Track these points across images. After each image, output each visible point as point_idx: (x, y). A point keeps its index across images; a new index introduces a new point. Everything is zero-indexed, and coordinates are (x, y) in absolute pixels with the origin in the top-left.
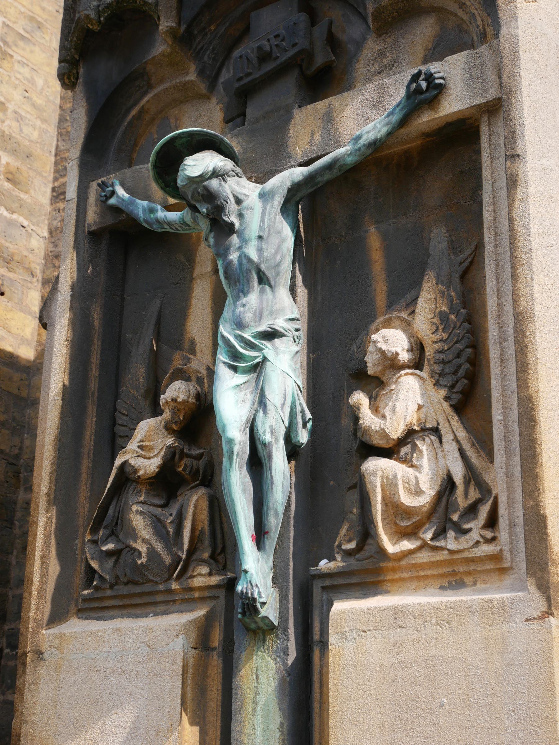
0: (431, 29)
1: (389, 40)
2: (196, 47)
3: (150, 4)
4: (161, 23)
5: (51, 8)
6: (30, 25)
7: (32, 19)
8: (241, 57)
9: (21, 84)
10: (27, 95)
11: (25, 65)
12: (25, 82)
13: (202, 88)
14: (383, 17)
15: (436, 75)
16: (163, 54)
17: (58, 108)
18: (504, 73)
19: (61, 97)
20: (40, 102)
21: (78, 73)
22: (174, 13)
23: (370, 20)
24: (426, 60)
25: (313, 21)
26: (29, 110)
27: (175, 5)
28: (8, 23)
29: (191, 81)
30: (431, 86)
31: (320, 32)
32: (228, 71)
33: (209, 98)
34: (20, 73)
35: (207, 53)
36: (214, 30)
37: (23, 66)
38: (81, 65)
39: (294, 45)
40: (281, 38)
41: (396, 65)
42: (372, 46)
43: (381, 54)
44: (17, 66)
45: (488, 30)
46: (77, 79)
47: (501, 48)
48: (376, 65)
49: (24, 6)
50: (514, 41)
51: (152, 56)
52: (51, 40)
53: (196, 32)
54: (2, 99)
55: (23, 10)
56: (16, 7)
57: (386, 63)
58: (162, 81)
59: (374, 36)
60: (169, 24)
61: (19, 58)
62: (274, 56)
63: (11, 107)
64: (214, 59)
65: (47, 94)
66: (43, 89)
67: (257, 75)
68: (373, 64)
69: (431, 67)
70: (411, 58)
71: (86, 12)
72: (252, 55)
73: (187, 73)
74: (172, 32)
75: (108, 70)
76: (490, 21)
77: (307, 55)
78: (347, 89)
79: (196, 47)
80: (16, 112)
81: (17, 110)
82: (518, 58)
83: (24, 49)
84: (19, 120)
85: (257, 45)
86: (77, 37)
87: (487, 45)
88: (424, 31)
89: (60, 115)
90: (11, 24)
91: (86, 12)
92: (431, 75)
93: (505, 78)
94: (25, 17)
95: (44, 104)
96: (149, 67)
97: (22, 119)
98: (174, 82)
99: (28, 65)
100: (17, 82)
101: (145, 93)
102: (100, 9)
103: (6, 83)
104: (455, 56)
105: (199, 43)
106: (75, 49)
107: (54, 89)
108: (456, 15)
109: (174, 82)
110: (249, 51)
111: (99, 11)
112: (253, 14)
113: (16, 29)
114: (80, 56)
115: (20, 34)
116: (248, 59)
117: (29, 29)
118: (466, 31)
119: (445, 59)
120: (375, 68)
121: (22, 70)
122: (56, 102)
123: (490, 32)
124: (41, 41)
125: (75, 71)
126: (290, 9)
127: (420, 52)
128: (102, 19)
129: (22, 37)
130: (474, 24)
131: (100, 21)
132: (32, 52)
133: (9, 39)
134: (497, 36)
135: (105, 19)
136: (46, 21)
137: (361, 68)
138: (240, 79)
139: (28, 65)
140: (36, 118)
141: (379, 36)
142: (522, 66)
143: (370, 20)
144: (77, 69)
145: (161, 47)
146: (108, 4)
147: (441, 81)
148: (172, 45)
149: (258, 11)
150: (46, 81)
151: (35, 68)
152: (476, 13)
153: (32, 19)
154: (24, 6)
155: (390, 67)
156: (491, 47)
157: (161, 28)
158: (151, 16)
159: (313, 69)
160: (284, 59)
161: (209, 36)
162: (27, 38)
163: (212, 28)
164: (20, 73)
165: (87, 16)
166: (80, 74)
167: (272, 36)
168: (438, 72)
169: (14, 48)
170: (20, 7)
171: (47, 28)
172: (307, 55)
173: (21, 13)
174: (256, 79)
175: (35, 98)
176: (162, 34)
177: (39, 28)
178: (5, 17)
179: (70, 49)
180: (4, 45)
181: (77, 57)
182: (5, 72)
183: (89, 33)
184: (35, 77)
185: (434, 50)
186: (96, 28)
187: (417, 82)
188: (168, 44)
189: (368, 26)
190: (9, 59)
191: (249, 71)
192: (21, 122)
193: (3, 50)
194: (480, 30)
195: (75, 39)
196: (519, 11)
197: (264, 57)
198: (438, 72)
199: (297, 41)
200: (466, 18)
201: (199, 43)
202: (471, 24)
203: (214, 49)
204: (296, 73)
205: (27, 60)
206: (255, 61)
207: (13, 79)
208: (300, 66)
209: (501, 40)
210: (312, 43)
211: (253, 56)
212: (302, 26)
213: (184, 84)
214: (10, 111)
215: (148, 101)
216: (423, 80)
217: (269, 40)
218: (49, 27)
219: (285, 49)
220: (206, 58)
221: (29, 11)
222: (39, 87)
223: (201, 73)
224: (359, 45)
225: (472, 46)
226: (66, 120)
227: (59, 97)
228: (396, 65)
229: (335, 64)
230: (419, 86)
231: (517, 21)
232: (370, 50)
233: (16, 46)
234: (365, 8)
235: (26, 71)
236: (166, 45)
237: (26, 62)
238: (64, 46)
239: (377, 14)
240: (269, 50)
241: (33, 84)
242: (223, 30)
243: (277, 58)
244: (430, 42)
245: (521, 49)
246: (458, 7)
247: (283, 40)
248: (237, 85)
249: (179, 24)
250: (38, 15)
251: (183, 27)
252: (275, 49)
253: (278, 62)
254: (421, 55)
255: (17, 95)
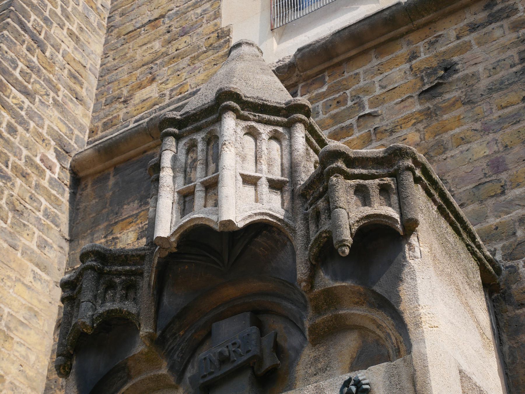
0: (355, 342)
1: (322, 349)
2: (168, 348)
3: (133, 314)
4: (141, 329)
5: (45, 301)
6: (29, 314)
7: (30, 309)
8: (205, 359)
9: (18, 360)
10: (22, 368)
11: (22, 346)
12: (22, 359)
13: (172, 380)
14: (317, 332)
15: (363, 382)
16: (141, 353)
17: (45, 378)
18: (418, 383)
19: (48, 369)
20: (31, 373)
21: (71, 365)
22: (152, 322)
23: (307, 333)
24: (353, 368)
25: (262, 333)
26: (22, 381)
27: (153, 315)
28: (12, 313)
29: (163, 375)
30: (359, 390)
31: (267, 342)
32: (193, 367)
33: (177, 388)
34: (18, 352)
35: (177, 353)
36: (183, 335)
37: (20, 346)
38: (74, 358)
39: (248, 351)
40: (237, 345)
41: (328, 369)
42: (308, 353)
43: (316, 359)
44: (16, 346)
45: (401, 346)
46: (70, 369)
47: (414, 363)
48: (312, 368)
49: (25, 299)
50: (424, 358)
51: (133, 354)
52: (43, 324)
53: (168, 337)
54: (2, 373)
55: (24, 302)
56: (19, 301)
57: (320, 367)
58: (139, 373)
59: (310, 345)
60: (148, 331)
61: (18, 340)
62: (232, 359)
63: (8, 379)
64: (182, 357)
65: (38, 367)
66: (34, 364)
67: (218, 374)
68: (310, 368)
69: (359, 375)
70: (340, 364)
71: (82, 320)
72: (214, 358)
73: (160, 368)
74: (150, 337)
75: (96, 363)
76: (402, 339)
77: (258, 359)
78: (291, 389)
79: (168, 348)
80: (11, 383)
81: (13, 381)
82: (428, 372)
83: (22, 333)
84: (14, 389)
85: (220, 350)
86: (73, 337)
87: (401, 359)
88: (349, 344)
89: (46, 384)
90: (14, 314)
91: (82, 320)
92: (359, 381)
93: (418, 387)
94: (25, 308)
95: (35, 375)
96: (131, 363)
97: (16, 388)
98: (149, 375)
99: (24, 345)
100: (15, 359)
101: (125, 382)
102: (94, 317)
103: (7, 360)
104: (377, 366)
105: (171, 344)
106: (71, 346)
107: (43, 364)
108: (374, 332)
109: (149, 375)
110: (212, 355)
111: (93, 319)
112: (214, 325)
113: (18, 317)
114: (75, 351)
115: (20, 321)
116: (211, 361)
117: (27, 316)
118: (383, 345)
119: (369, 368)
120: (312, 370)
121: (19, 349)
122: (44, 373)
123: (403, 348)
124: (36, 326)
125: (69, 363)
126: (244, 322)
127: (347, 359)
128: (95, 325)
129: (22, 324)
130: (389, 341)
131: (93, 327)
132: (28, 334)
133: (12, 325)
134: (409, 351)
135: (97, 325)
136: (41, 310)
137: (301, 370)
138: (205, 376)
139: (24, 345)
140: (28, 387)
141: (314, 345)
142: (431, 378)
143: (307, 333)
144: (71, 361)
145: (140, 348)
146: (100, 314)
147: (367, 387)
148: (149, 346)
149: (218, 322)
150: (38, 357)
151: (29, 347)
152: (391, 333)
153: (30, 309)
154: (25, 299)
155: (324, 370)
156: (405, 361)
157: (141, 333)
158: (132, 323)
159: (263, 370)
160: (240, 362)
161: (178, 339)
162: (26, 324)
163: (181, 333)
164: (18, 352)
165: (84, 323)
166: (73, 365)
167: (230, 344)
168: (364, 379)
169: (15, 332)
170: (22, 300)
171: (42, 316)
172: (258, 359)
173: (23, 305)
174: (218, 377)
175: (28, 371)
176: (142, 338)
177: (35, 316)
178: (10, 308)
179: (67, 346)
180: (7, 329)
181: (72, 352)
182: (6, 352)
183: (83, 335)
184: (29, 354)
185: (358, 359)
186: (90, 332)
187: (348, 387)
188: (146, 345)
189: (305, 338)
190: (10, 341)
191: (211, 370)
192: (16, 391)
193: (6, 333)
194: (395, 346)
195: (71, 338)
196: (425, 334)
197: (224, 360)
198: (364, 379)
199: (250, 349)
200: (382, 335)
201: (171, 344)
202: (387, 341)
203: (182, 349)
204: (249, 373)
205: (24, 341)
206: (217, 363)
207: (12, 356)
208: (253, 368)
209: (413, 357)
210: (261, 350)
211: (215, 359)
212: (254, 337)
213: (157, 377)
214: (7, 382)
215: (127, 389)
216: (352, 385)
217: (227, 347)
218: (43, 315)
219: (241, 354)
220: (175, 357)
221: (29, 303)
222: (32, 362)
223: (171, 368)
224: (298, 352)
225: (388, 359)
226: (52, 388)
227: (47, 369)
228: (328, 369)
229: (280, 367)
230: (350, 390)
231: (424, 342)
232: (307, 356)
233: (17, 330)
234: (303, 324)
235: (22, 350)
236: (144, 346)
237: (23, 342)
238: (62, 344)
239: (312, 330)
240: (228, 354)
241: (27, 360)
242: (190, 335)
243: (234, 361)
244: (355, 352)
245: (430, 364)
246: (376, 327)
247: (239, 347)
248: (201, 381)
249: (155, 330)
250: (35, 306)
251: (159, 333)
252: (233, 354)
253: (235, 364)
254: (348, 362)
255: (14, 370)
